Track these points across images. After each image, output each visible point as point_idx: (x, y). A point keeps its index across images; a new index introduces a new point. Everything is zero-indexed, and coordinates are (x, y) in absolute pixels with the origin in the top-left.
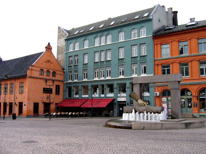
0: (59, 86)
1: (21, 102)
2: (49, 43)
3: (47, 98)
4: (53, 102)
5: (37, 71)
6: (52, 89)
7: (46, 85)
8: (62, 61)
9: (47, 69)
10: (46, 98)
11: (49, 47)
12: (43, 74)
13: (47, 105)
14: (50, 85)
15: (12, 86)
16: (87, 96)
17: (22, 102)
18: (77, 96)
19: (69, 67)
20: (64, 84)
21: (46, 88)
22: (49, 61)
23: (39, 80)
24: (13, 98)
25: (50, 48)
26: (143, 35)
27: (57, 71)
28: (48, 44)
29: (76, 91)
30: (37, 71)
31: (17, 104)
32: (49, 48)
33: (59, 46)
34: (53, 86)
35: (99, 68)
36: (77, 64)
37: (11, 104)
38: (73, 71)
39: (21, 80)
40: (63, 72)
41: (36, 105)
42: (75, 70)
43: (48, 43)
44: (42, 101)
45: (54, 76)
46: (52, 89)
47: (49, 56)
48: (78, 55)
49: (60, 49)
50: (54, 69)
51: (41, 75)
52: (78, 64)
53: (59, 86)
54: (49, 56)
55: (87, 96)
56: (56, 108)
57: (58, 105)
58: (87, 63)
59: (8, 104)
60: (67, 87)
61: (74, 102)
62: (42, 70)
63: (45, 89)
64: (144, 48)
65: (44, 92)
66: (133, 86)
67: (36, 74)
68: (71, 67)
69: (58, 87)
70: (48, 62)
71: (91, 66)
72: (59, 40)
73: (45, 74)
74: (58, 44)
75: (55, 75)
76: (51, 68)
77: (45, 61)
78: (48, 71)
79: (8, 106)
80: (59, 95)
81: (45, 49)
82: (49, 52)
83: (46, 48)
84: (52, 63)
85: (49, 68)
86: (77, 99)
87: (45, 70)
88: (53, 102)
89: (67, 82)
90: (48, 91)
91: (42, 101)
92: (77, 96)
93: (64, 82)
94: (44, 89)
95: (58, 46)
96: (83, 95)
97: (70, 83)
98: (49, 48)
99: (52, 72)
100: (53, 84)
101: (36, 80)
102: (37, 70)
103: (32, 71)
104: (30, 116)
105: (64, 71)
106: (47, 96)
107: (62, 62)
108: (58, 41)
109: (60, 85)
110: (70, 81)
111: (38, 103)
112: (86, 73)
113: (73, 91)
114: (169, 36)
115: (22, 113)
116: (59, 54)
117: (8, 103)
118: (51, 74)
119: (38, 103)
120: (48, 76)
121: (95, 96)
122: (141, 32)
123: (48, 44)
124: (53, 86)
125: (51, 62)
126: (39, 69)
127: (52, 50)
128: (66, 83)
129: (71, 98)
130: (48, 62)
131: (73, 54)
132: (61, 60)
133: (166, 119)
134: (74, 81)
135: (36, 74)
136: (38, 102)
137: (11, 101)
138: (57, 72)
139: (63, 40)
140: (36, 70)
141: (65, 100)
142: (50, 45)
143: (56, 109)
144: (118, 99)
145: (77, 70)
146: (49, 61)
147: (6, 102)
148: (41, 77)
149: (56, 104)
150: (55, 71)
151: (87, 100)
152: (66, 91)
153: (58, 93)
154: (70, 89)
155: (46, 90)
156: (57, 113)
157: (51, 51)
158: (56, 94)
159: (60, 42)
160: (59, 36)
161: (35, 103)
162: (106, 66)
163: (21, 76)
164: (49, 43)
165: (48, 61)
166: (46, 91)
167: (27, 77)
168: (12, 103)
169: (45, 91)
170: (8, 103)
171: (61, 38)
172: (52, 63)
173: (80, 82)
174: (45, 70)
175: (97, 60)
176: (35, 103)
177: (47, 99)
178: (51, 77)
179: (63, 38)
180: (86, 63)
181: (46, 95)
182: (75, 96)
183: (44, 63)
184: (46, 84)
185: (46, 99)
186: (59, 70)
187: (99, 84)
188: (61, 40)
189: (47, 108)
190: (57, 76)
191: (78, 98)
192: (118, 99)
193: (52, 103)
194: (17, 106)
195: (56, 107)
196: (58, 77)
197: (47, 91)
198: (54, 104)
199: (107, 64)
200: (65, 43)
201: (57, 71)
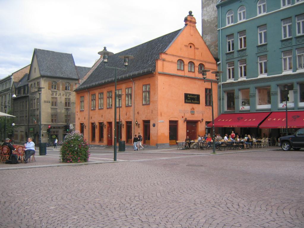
1: (146, 119)
2: (190, 13)
3: (191, 112)
4: (202, 120)
5: (172, 62)
6: (198, 96)
8: (213, 46)
9: (190, 59)
10: (190, 111)
11: (191, 19)
12: (183, 69)
13: (192, 125)
15: (94, 98)
16: (267, 106)
17: (149, 120)
18: (247, 108)
19: (227, 54)
20: (219, 87)
21: (190, 94)
22: (192, 46)
23: (176, 79)
24: (132, 113)
25: (193, 20)
27: (205, 62)
29: (242, 99)
30: (172, 62)
31: (139, 125)
32: (191, 21)
33: (204, 20)
37: (101, 125)
39: (146, 81)
40: (215, 66)
41: (173, 126)
42: (240, 59)
43: (189, 13)
44: (184, 118)
46: (198, 96)
48: (233, 34)
49: (207, 25)
50: (202, 59)
51: (180, 70)
54: (192, 35)
55: (267, 106)
56: (207, 130)
57: (209, 124)
59: (97, 126)
60: (224, 92)
61: (242, 118)
62: (181, 61)
65: (187, 101)
66: (270, 97)
67: (172, 68)
69: (209, 92)
70: (191, 47)
72: (205, 9)
73: (187, 68)
74: (202, 16)
78: (191, 63)
79: (123, 127)
81: (184, 23)
82: (192, 27)
83: (186, 20)
84: (197, 49)
85: (193, 57)
86: (247, 113)
87: (186, 61)
88: (202, 120)
89: (225, 82)
91: (183, 117)
92: (247, 108)
93: (220, 83)
94: (186, 95)
96: (259, 105)
97: (231, 84)
98: (189, 20)
101: (171, 79)
102: (173, 61)
103: (165, 63)
104: (164, 144)
105: (218, 63)
106: (191, 108)
107: (213, 48)
108: (202, 11)
110: (232, 80)
111: (176, 122)
113: (238, 98)
115: (149, 139)
116: (206, 34)
117: (124, 123)
118: (197, 69)
119: (176, 122)
120: (191, 71)
121: (243, 108)
123: (189, 14)
125: (196, 47)
126: (176, 59)
127: (196, 25)
128: (222, 84)
129: (234, 112)
130: (191, 47)
131: (235, 31)
132: (210, 44)
134: (240, 80)
135: (172, 68)
136: (176, 119)
137: (129, 118)
140: (171, 60)
141: (222, 115)
142: (192, 16)
143: (207, 132)
145: (244, 58)
146: (192, 46)
147: (120, 121)
148: (180, 73)
149: (207, 123)
150: (204, 63)
151: (269, 114)
152: (223, 99)
153: (209, 102)
155: (190, 98)
158: (206, 105)
160: (205, 2)
161: (171, 122)
163: (109, 81)
164: (190, 13)
167: (155, 74)
168: (131, 122)
169: (188, 100)
170: (124, 123)
171: (208, 5)
172: (197, 49)
173: (251, 80)
174: (186, 61)
176: (171, 122)
177: (192, 114)
179: (212, 5)
181: (189, 106)
182: (241, 107)
183: (185, 49)
185: (190, 114)
186: (209, 61)
187: (295, 81)
188: (208, 8)
191: (249, 111)
193: (199, 121)
194: (139, 127)
195: (206, 128)
197: (191, 99)
198: (204, 123)
200: (216, 13)
201: (205, 62)
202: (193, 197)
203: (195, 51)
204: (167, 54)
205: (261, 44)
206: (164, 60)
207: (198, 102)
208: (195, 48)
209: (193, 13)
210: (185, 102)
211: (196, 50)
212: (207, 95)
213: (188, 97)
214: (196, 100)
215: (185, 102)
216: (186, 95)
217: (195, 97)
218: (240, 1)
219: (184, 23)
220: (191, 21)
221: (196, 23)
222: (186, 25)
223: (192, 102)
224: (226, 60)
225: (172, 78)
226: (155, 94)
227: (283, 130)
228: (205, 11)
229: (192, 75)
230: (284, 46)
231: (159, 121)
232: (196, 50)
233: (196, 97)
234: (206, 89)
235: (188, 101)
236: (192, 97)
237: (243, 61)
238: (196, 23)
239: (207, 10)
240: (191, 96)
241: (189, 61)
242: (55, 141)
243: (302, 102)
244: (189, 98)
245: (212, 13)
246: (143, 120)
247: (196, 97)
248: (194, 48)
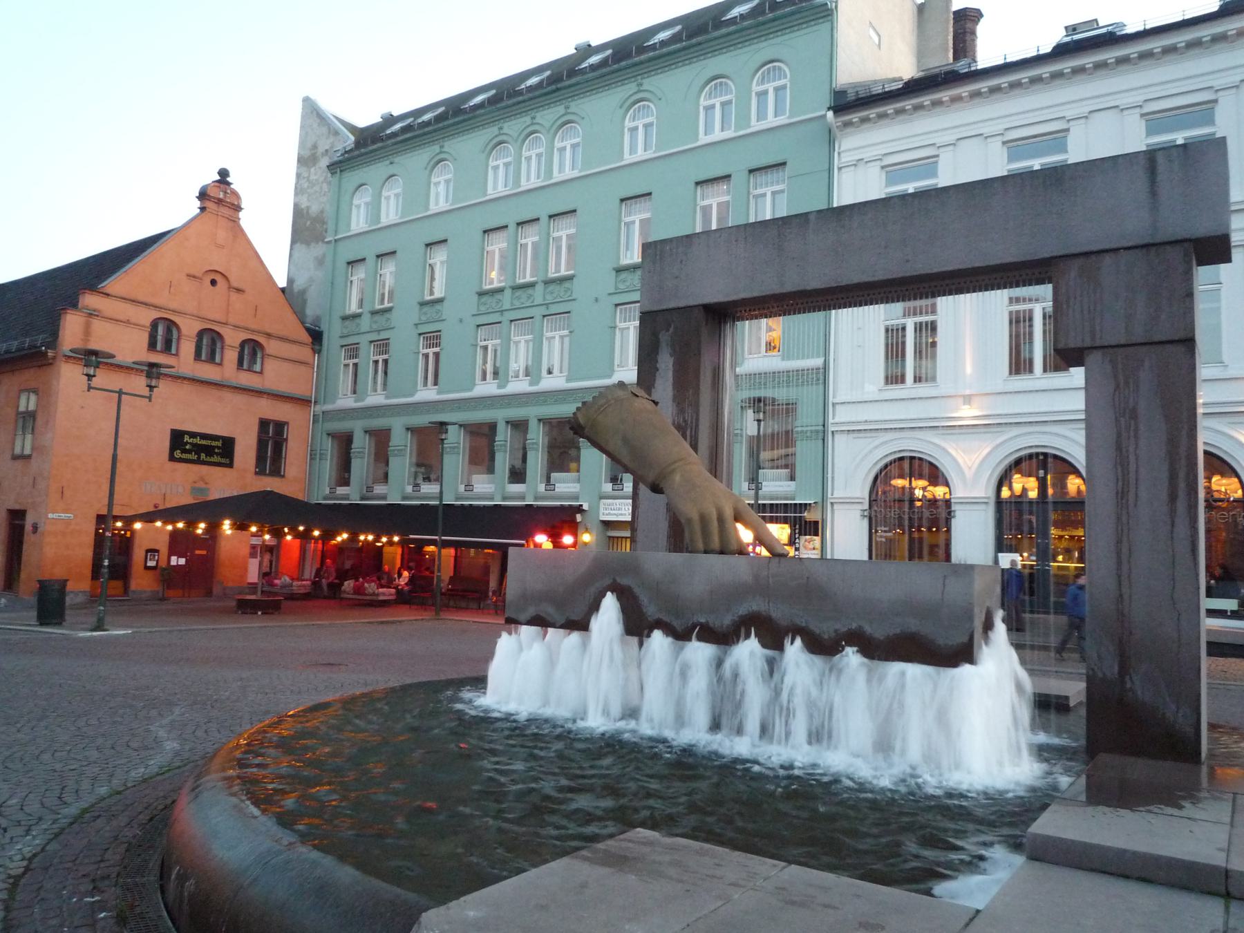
0: (280, 426)
1: (17, 507)
2: (224, 173)
7: (90, 388)
14: (120, 393)
26: (798, 511)
28: (218, 178)
34: (150, 398)
35: (506, 323)
36: (386, 305)
38: (363, 340)
42: (374, 337)
43: (219, 173)
45: (211, 359)
47: (223, 247)
52: (391, 305)
53: (280, 426)
58: (443, 295)
63: (187, 438)
64: (774, 193)
65: (178, 454)
68: (357, 321)
70: (213, 282)
71: (460, 309)
74: (296, 194)
75: (218, 350)
76: (231, 320)
77: (193, 272)
80: (283, 476)
81: (198, 203)
83: (203, 195)
84: (239, 290)
85: (217, 317)
90: (209, 451)
94: (177, 438)
95: (296, 206)
99: (237, 344)
100: (151, 387)
102: (133, 320)
109: (287, 423)
112: (434, 353)
114: (921, 113)
122: (756, 197)
123: (218, 178)
124: (150, 398)
126: (147, 316)
127: (241, 214)
130: (213, 282)
133: (436, 387)
138: (272, 347)
139: (319, 171)
142: (229, 184)
144: (602, 511)
145: (383, 335)
154: (344, 441)
155: (194, 445)
156: (357, 580)
157: (235, 222)
159: (306, 185)
162: (543, 311)
164: (224, 173)
165: (213, 276)
166: (189, 452)
167: (54, 358)
169: (184, 451)
175: (494, 278)
178: (228, 369)
180: (438, 294)
184: (90, 377)
189: (182, 561)
190: (270, 365)
192: (602, 506)
196: (275, 375)
199: (549, 299)
201: (269, 335)
202: (15, 787)
203: (229, 296)
204: (108, 295)
205: (432, 297)
206: (92, 314)
207: (227, 461)
208: (230, 287)
209: (231, 174)
210: (172, 458)
211: (234, 296)
212: (268, 441)
213: (187, 443)
214: (217, 454)
215: (172, 458)
216: (177, 438)
217: (214, 444)
218: (388, 162)
219: (193, 207)
220: (219, 202)
221: (241, 209)
222: (203, 209)
223: (199, 458)
224: (341, 337)
225: (280, 389)
226: (47, 422)
227: (1057, 584)
228: (304, 178)
229: (207, 371)
230: (483, 309)
231: (50, 516)
232: (232, 293)
233: (219, 444)
234: (264, 424)
235: (185, 456)
236: (204, 442)
237: (383, 346)
238: (241, 209)
239: (308, 177)
240: (198, 441)
241: (198, 326)
242: (411, 580)
243: (513, 483)
244: (187, 447)
245: (321, 188)
246: (9, 508)
247: (219, 444)
248: (227, 286)
